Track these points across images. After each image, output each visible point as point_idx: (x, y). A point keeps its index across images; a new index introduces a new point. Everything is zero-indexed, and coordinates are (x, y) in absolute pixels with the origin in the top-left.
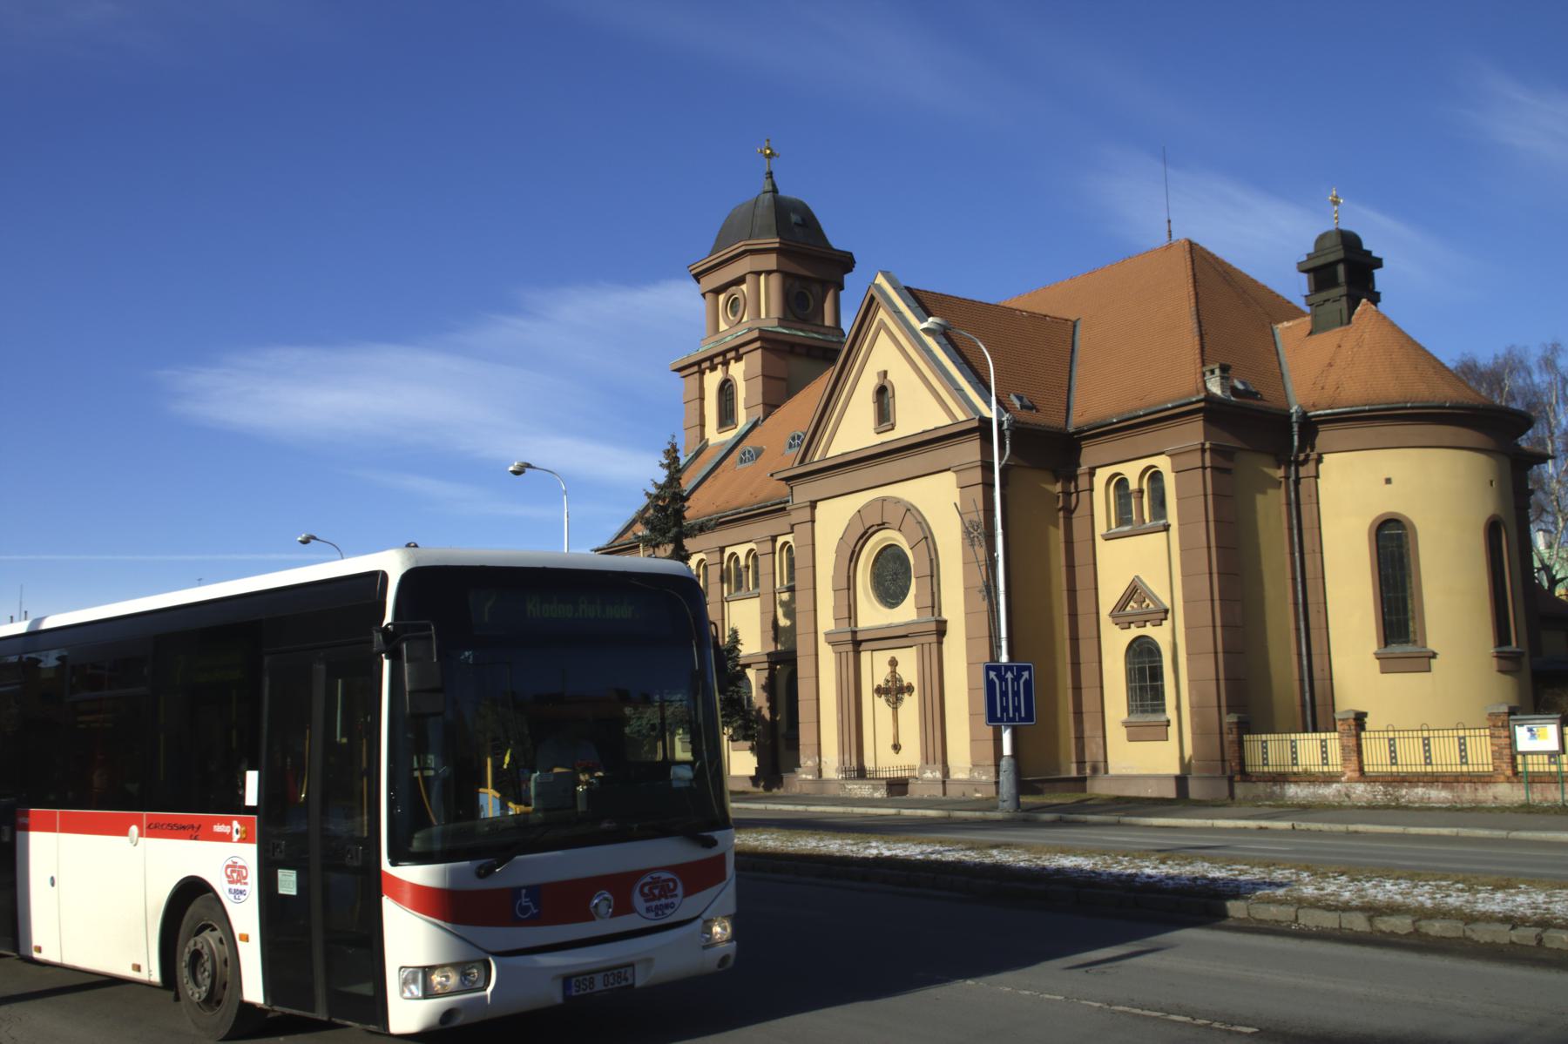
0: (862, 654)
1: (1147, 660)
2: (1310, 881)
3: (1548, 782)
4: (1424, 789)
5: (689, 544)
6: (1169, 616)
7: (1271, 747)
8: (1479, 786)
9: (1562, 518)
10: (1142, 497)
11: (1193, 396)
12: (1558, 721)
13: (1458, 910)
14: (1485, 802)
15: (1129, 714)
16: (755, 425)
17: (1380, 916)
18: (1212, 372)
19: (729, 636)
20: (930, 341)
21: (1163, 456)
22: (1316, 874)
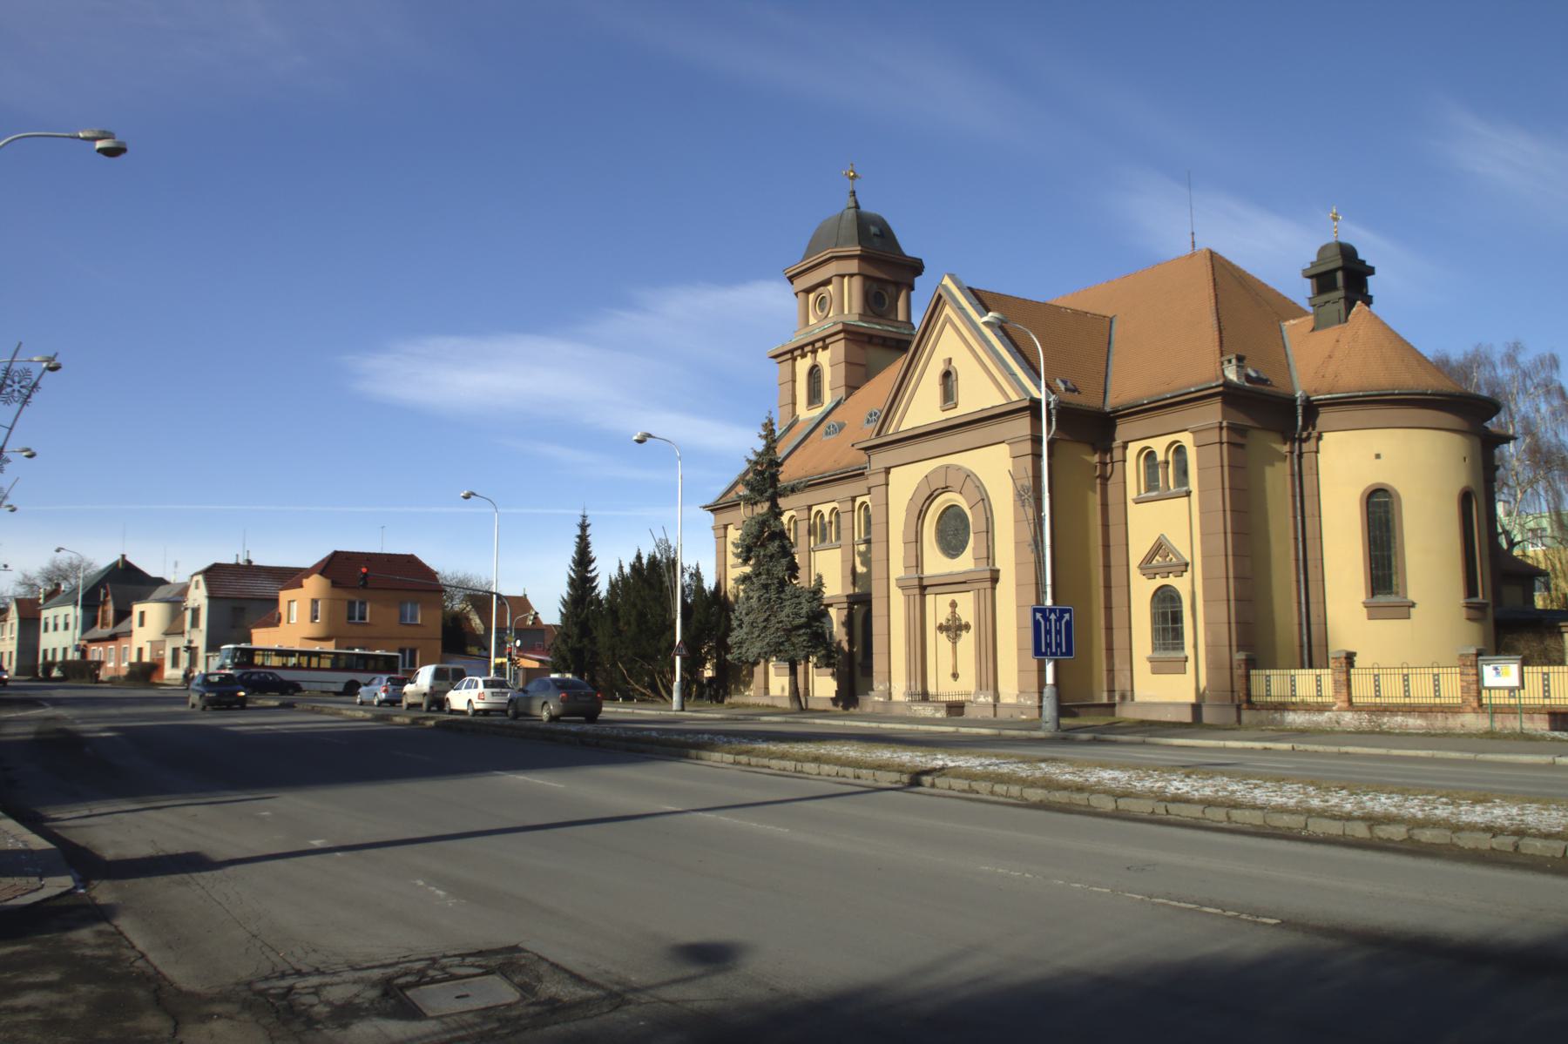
0: (928, 597)
1: (1169, 605)
2: (1315, 794)
3: (1508, 713)
4: (1402, 718)
5: (782, 502)
6: (1189, 568)
7: (1274, 680)
8: (1449, 715)
9: (1521, 490)
10: (1167, 467)
11: (1213, 382)
12: (1519, 662)
13: (1446, 820)
14: (1454, 729)
15: (1153, 651)
16: (838, 404)
17: (1379, 824)
18: (1230, 361)
19: (815, 580)
20: (987, 332)
21: (1186, 432)
22: (1320, 788)
